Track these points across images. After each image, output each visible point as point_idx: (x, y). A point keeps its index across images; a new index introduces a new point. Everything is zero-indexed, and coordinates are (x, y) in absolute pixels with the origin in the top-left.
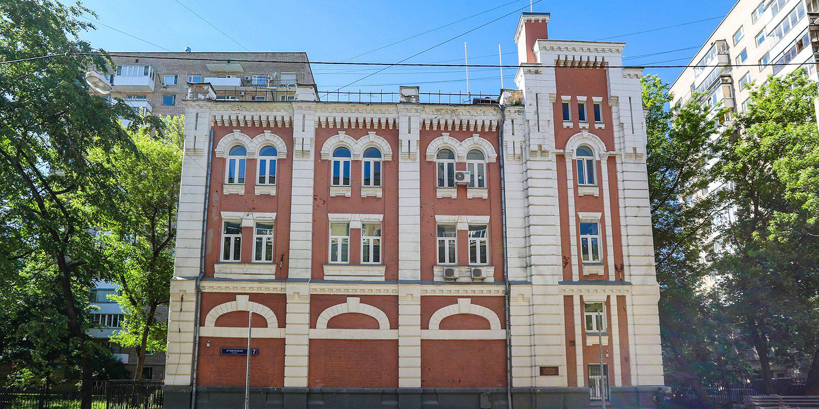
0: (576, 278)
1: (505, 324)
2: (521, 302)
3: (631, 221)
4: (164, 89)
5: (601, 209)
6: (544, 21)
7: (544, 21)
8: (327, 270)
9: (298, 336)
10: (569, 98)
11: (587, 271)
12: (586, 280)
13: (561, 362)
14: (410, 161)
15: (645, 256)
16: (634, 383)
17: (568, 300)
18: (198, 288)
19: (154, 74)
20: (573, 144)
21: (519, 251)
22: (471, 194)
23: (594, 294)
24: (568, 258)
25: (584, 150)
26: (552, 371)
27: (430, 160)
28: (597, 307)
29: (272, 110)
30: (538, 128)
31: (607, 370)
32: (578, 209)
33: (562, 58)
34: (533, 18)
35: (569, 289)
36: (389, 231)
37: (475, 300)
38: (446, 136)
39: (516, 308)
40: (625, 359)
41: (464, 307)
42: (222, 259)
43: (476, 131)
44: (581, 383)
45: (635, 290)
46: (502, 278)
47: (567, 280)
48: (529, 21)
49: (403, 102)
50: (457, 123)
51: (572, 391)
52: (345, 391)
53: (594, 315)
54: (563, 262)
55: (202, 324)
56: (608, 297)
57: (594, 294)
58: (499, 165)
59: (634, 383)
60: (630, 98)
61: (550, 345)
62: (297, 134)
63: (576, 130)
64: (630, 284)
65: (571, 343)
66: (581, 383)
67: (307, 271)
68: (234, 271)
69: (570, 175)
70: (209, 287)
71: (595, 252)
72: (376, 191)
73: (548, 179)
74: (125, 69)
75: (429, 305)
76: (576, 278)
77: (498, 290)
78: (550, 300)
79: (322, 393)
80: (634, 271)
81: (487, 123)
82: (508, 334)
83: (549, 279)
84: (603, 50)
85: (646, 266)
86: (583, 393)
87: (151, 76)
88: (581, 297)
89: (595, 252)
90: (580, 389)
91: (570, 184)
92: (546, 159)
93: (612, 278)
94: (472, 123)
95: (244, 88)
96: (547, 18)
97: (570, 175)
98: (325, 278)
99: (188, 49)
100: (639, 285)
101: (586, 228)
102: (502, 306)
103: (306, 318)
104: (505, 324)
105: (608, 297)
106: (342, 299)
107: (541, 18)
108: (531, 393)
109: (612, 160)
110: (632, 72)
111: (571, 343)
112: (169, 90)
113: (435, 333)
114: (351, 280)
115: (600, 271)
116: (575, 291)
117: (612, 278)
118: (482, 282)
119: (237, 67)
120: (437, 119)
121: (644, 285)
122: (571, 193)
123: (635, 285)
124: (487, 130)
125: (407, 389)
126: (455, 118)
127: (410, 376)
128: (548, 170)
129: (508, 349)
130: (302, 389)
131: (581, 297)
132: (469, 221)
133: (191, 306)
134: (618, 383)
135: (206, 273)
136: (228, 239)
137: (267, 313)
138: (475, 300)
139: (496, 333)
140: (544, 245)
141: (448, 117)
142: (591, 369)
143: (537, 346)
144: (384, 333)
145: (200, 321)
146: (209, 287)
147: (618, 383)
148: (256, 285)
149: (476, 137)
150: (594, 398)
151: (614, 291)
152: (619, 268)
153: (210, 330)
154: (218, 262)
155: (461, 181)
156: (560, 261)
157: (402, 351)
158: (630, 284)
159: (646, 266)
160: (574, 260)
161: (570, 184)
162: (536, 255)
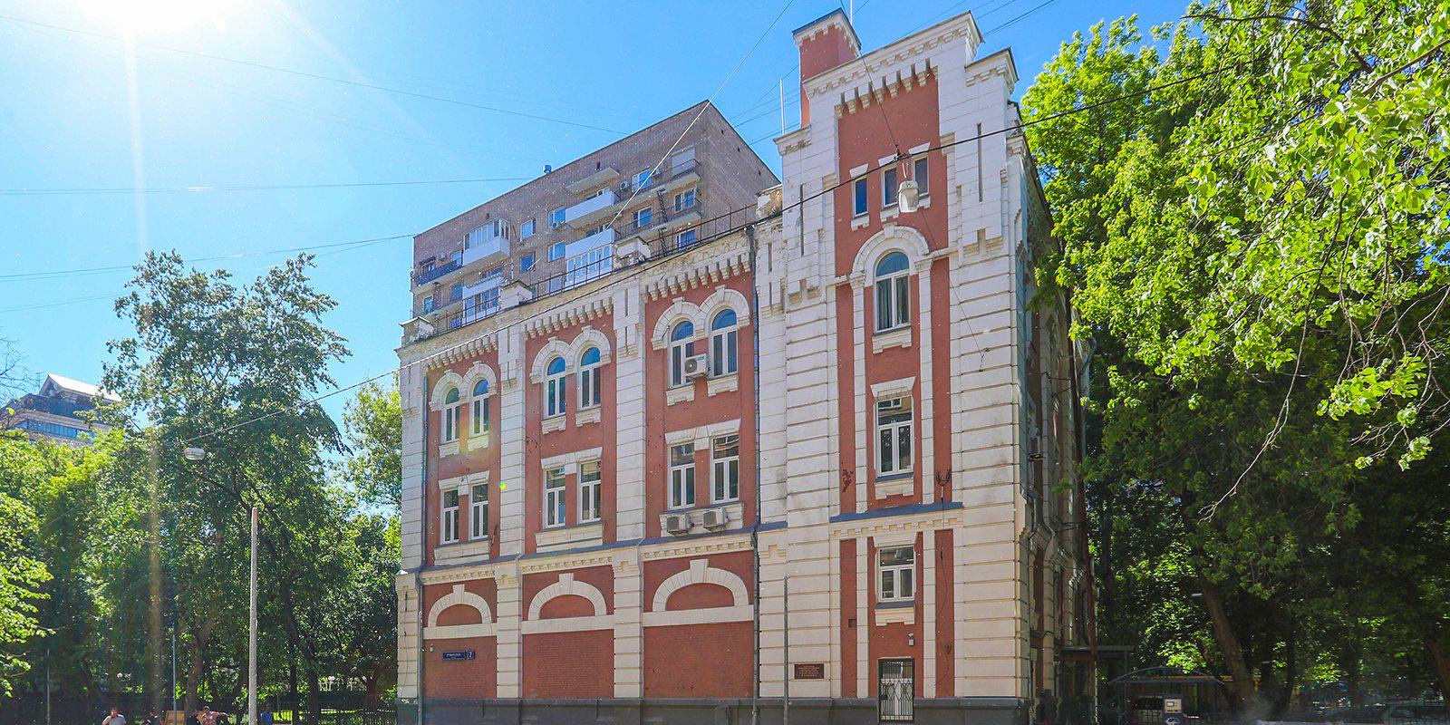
0: (861, 507)
1: (755, 598)
2: (775, 558)
3: (973, 380)
4: (522, 248)
5: (915, 371)
6: (832, 28)
7: (832, 28)
8: (541, 539)
9: (626, 624)
10: (863, 169)
11: (882, 491)
12: (880, 508)
13: (831, 657)
14: (629, 358)
15: (996, 446)
16: (962, 689)
17: (848, 547)
18: (418, 581)
19: (507, 228)
20: (867, 259)
21: (778, 471)
22: (714, 388)
23: (895, 532)
24: (852, 473)
25: (894, 260)
26: (815, 671)
27: (659, 348)
28: (905, 554)
29: (477, 333)
30: (803, 248)
31: (914, 667)
32: (871, 379)
33: (850, 97)
34: (811, 33)
35: (846, 529)
36: (605, 474)
37: (716, 560)
38: (678, 302)
39: (769, 571)
40: (946, 649)
41: (699, 572)
42: (443, 541)
43: (721, 281)
44: (863, 691)
45: (967, 516)
46: (754, 525)
47: (848, 513)
48: (807, 40)
49: (620, 269)
50: (692, 276)
51: (846, 705)
52: (556, 703)
53: (897, 570)
54: (842, 480)
55: (424, 625)
56: (920, 534)
57: (895, 532)
58: (753, 329)
59: (962, 689)
60: (979, 125)
61: (812, 628)
62: (502, 359)
63: (876, 227)
64: (960, 506)
65: (849, 623)
66: (863, 691)
67: (518, 545)
68: (452, 555)
69: (859, 319)
70: (431, 578)
71: (904, 451)
72: (592, 415)
73: (819, 336)
74: (474, 237)
75: (653, 574)
76: (861, 507)
77: (741, 543)
78: (816, 550)
79: (536, 706)
80: (970, 479)
81: (734, 262)
82: (757, 611)
83: (814, 516)
84: (927, 45)
85: (994, 466)
86: (864, 707)
87: (503, 235)
88: (870, 540)
89: (904, 451)
90: (929, 700)
91: (859, 336)
92: (817, 301)
93: (928, 499)
94: (712, 270)
95: (625, 205)
96: (838, 21)
97: (859, 319)
98: (539, 550)
99: (548, 168)
100: (976, 507)
101: (890, 411)
102: (746, 565)
103: (636, 599)
104: (755, 598)
105: (920, 534)
106: (552, 578)
107: (824, 27)
108: (776, 705)
109: (940, 267)
110: (983, 69)
111: (849, 623)
112: (527, 245)
113: (661, 617)
114: (549, 551)
115: (907, 488)
116: (860, 530)
117: (928, 499)
118: (723, 531)
119: (608, 173)
120: (663, 280)
121: (988, 505)
122: (859, 353)
123: (969, 508)
124: (736, 273)
125: (622, 700)
126: (689, 270)
127: (627, 682)
128: (819, 320)
129: (756, 636)
130: (513, 700)
131: (870, 540)
132: (710, 434)
133: (414, 603)
134: (930, 691)
135: (427, 564)
136: (477, 509)
137: (478, 602)
138: (716, 560)
139: (740, 611)
140: (809, 457)
141: (677, 271)
142: (882, 667)
143: (800, 626)
144: (598, 622)
145: (647, 606)
146: (431, 578)
147: (930, 691)
148: (468, 570)
149: (721, 290)
150: (888, 718)
151: (929, 524)
152: (943, 479)
153: (434, 632)
154: (438, 546)
155: (694, 373)
156: (836, 479)
157: (618, 646)
158: (960, 506)
159: (994, 466)
160: (861, 476)
161: (859, 336)
162: (795, 476)
